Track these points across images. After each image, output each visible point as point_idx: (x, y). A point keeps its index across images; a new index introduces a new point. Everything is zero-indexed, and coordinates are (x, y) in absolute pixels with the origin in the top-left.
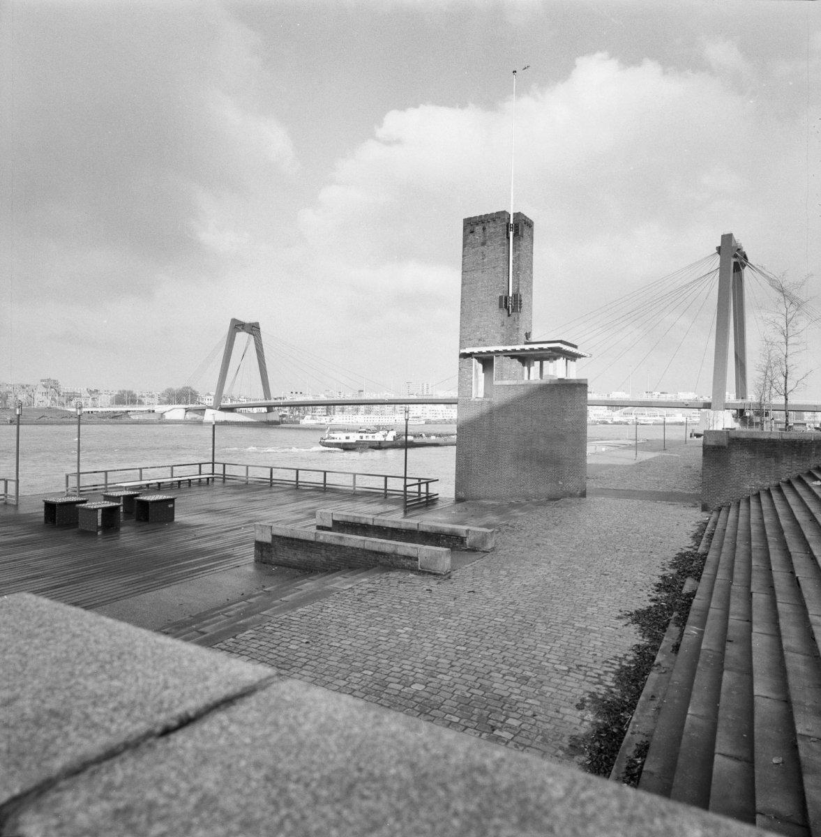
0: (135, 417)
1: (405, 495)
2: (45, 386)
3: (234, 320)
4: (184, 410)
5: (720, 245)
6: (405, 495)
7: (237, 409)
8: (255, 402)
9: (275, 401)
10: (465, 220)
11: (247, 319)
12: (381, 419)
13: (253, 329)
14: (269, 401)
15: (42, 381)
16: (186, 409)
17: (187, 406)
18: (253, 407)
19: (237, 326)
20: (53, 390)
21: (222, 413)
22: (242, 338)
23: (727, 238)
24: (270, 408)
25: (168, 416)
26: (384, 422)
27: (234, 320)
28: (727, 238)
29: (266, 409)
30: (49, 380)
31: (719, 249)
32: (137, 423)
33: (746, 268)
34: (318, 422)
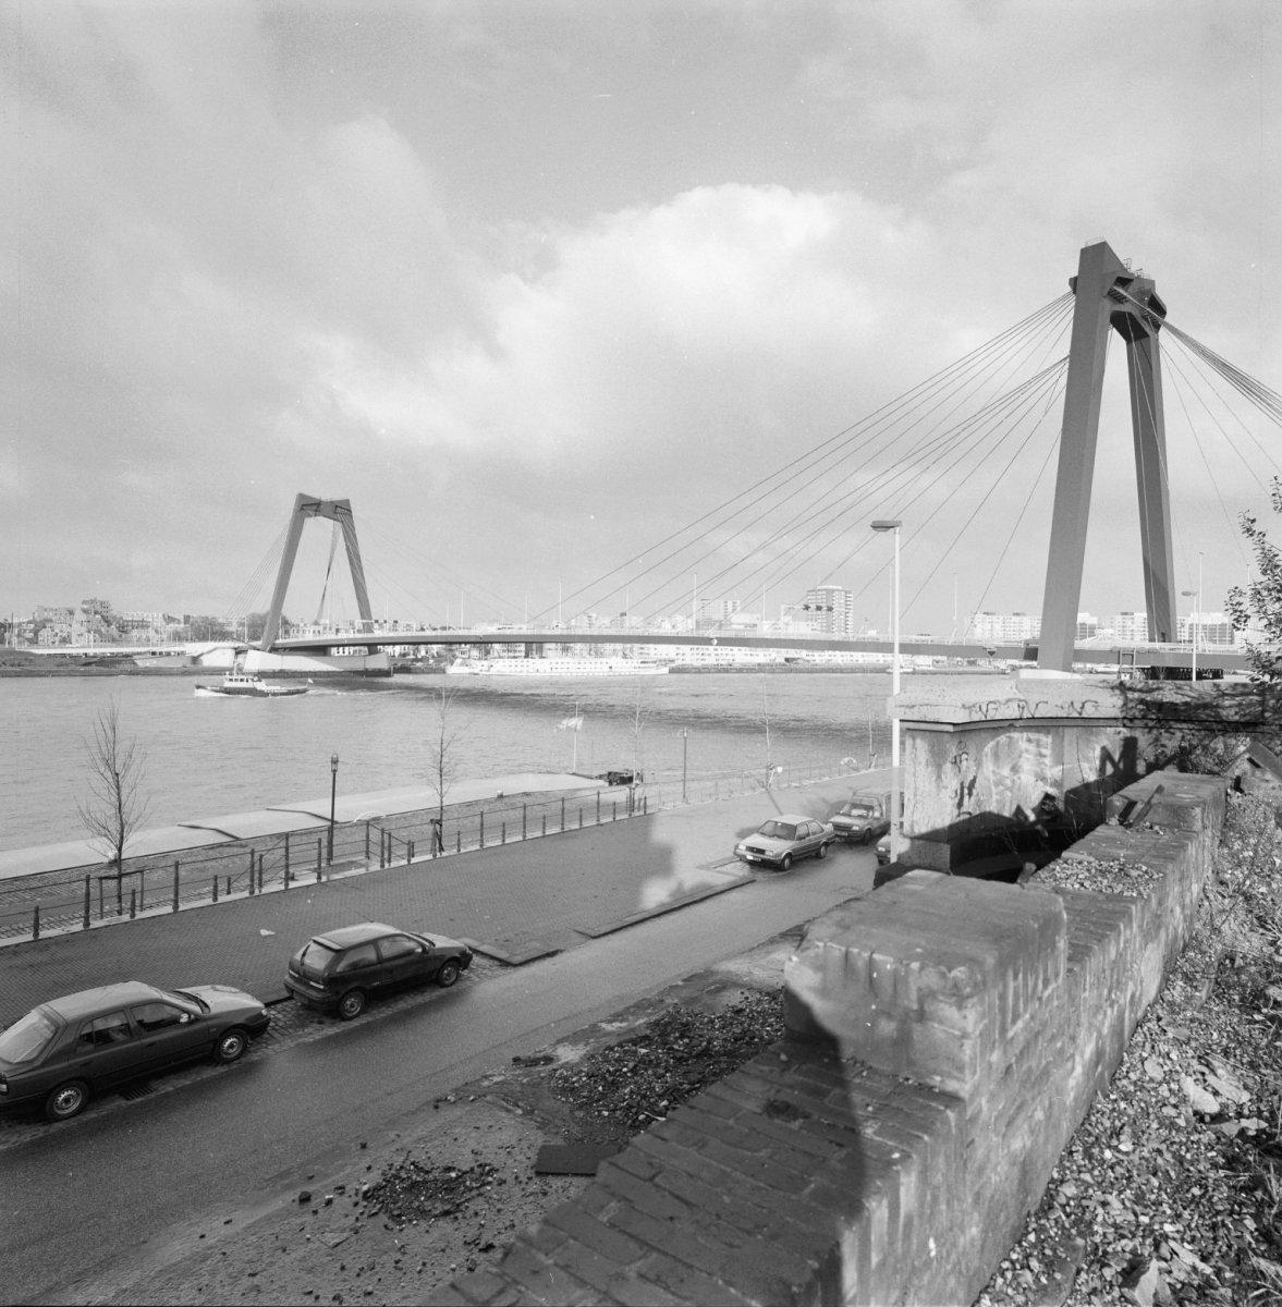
0: (141, 663)
1: (598, 803)
2: (85, 611)
3: (301, 496)
4: (234, 652)
5: (1075, 274)
6: (598, 803)
7: (334, 650)
8: (444, 633)
9: (434, 633)
10: (1084, 252)
11: (326, 494)
12: (582, 665)
13: (340, 511)
14: (369, 635)
15: (84, 602)
16: (235, 649)
17: (237, 645)
18: (394, 644)
19: (309, 506)
20: (98, 616)
21: (273, 656)
22: (319, 529)
23: (1096, 257)
24: (373, 647)
25: (207, 662)
26: (593, 670)
27: (301, 496)
28: (1096, 257)
29: (366, 649)
30: (93, 601)
31: (1074, 282)
32: (147, 672)
33: (1163, 331)
34: (472, 671)
